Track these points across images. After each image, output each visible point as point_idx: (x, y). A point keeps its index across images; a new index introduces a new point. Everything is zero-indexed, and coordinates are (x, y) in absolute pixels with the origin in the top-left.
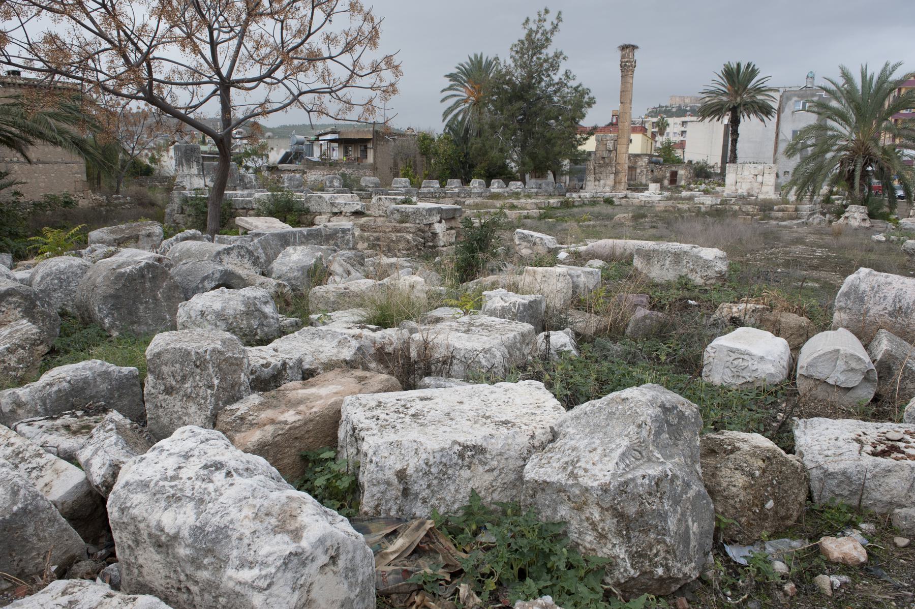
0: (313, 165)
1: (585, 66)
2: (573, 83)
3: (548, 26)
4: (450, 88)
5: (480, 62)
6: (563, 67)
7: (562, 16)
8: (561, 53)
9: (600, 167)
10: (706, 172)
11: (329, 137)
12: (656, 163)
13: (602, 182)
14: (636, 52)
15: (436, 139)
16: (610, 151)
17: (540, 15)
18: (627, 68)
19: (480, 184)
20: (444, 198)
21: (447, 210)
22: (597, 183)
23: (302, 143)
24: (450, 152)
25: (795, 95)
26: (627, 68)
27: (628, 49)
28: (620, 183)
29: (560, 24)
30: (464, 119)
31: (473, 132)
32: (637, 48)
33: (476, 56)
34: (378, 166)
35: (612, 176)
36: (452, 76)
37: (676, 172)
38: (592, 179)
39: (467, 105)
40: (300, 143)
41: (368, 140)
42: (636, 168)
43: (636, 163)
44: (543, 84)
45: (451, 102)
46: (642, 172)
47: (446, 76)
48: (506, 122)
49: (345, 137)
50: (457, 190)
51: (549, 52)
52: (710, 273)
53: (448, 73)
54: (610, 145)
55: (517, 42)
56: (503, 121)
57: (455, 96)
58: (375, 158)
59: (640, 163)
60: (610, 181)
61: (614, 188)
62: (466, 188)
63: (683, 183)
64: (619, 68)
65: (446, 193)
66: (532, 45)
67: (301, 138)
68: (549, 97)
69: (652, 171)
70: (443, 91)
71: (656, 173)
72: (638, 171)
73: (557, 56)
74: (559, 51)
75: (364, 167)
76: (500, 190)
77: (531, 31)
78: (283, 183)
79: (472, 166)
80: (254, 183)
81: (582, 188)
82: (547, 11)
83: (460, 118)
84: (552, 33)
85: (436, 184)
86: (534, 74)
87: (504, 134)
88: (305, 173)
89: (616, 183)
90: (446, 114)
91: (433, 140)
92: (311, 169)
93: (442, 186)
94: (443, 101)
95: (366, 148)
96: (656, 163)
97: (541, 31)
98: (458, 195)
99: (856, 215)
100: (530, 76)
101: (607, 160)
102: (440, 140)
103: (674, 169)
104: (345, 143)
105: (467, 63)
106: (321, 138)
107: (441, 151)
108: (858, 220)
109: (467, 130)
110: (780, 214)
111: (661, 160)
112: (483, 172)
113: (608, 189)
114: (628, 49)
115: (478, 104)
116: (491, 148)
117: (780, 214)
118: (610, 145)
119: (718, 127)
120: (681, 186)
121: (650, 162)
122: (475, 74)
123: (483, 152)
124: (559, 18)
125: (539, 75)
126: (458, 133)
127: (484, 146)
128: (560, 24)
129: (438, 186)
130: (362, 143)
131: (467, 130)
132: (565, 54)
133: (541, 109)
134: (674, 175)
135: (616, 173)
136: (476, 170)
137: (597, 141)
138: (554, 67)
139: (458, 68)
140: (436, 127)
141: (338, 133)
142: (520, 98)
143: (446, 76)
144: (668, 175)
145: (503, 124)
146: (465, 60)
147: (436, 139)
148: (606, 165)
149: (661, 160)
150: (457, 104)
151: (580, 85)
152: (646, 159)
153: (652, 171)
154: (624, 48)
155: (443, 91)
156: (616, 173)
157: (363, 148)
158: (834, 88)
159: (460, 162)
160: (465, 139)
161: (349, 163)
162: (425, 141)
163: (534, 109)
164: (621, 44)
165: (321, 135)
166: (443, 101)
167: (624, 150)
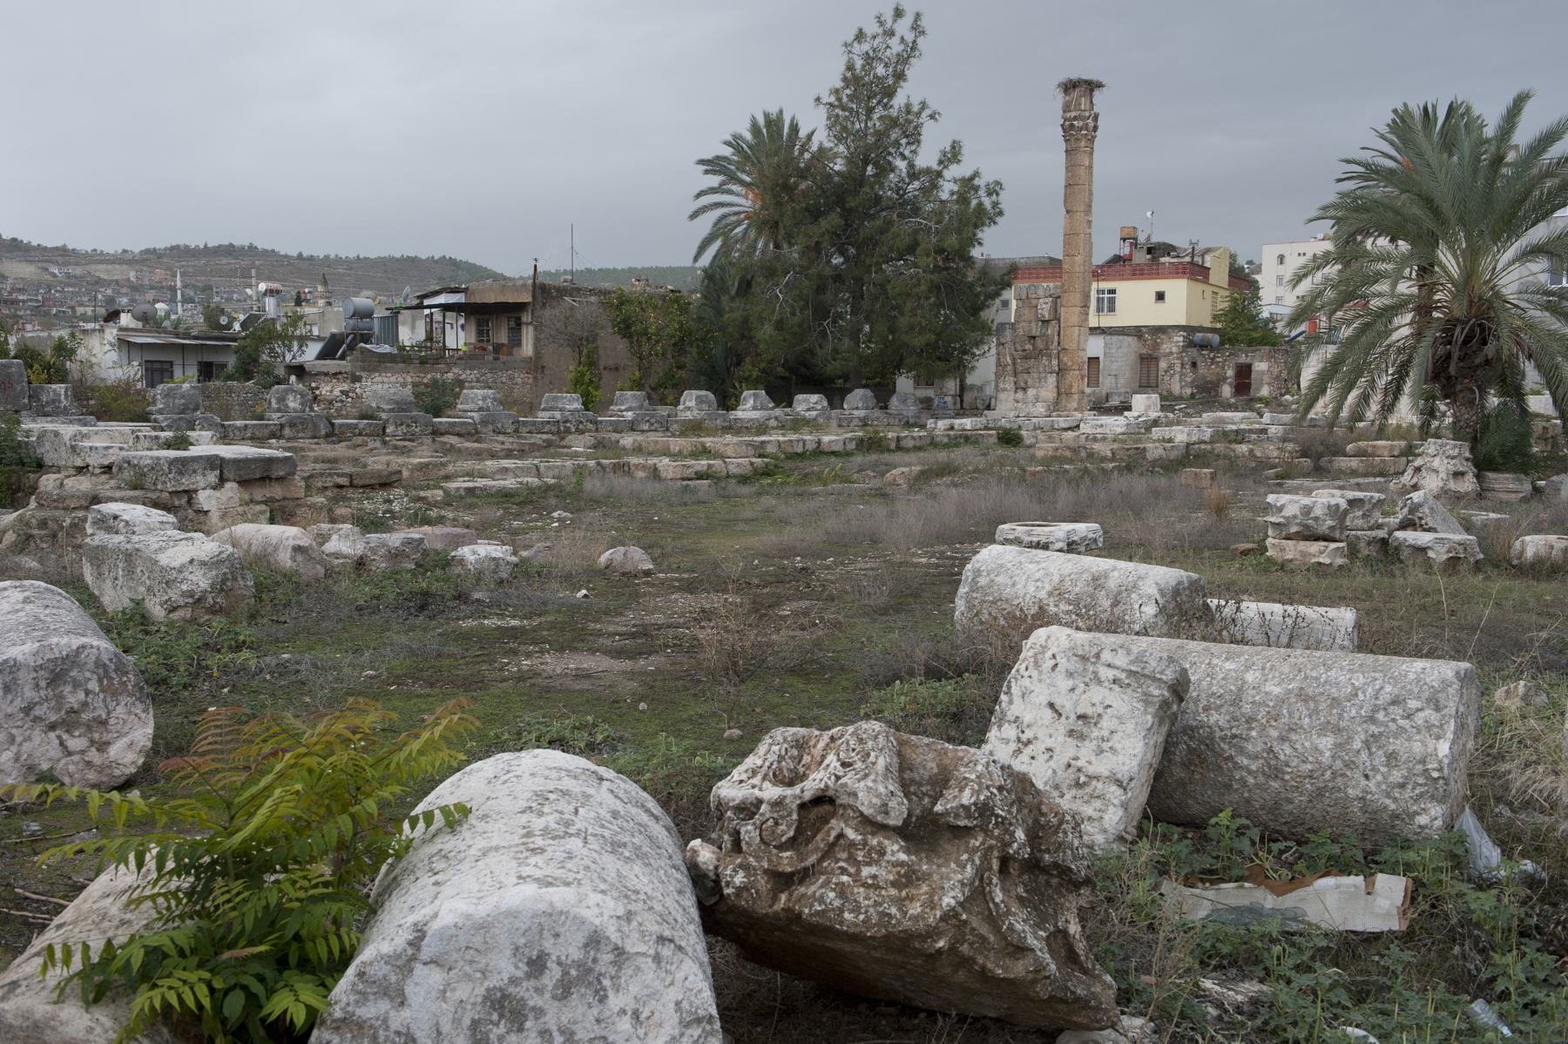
0: (379, 363)
1: (981, 131)
7: (923, 23)
8: (924, 106)
9: (1026, 358)
11: (442, 299)
12: (1203, 346)
13: (1031, 392)
14: (1098, 96)
17: (881, 23)
18: (1079, 133)
19: (700, 400)
21: (236, 462)
22: (1020, 395)
23: (368, 314)
26: (1079, 133)
29: (920, 40)
32: (1100, 85)
35: (1052, 379)
36: (713, 165)
41: (520, 307)
42: (1156, 359)
43: (1156, 346)
46: (1171, 367)
49: (478, 299)
50: (629, 415)
52: (174, 595)
53: (709, 156)
57: (722, 205)
59: (1166, 347)
60: (1048, 390)
61: (1056, 406)
63: (1265, 391)
66: (868, 89)
69: (1194, 365)
70: (699, 195)
71: (1202, 370)
72: (1163, 365)
78: (154, 402)
80: (64, 403)
82: (898, 13)
86: (873, 153)
88: (359, 379)
89: (1062, 393)
92: (371, 370)
95: (519, 324)
96: (1203, 346)
99: (1436, 463)
101: (1040, 344)
103: (1243, 359)
104: (480, 314)
106: (426, 302)
108: (1443, 475)
110: (1354, 463)
111: (1216, 338)
113: (1040, 409)
114: (1080, 88)
117: (1354, 463)
118: (1045, 308)
120: (1260, 400)
121: (1190, 344)
122: (767, 157)
124: (916, 28)
129: (577, 405)
130: (511, 312)
132: (933, 105)
134: (1244, 372)
135: (1061, 372)
141: (465, 291)
143: (702, 162)
144: (1230, 373)
148: (1037, 354)
149: (1216, 338)
152: (1179, 339)
153: (1194, 365)
154: (1069, 86)
155: (699, 195)
156: (1061, 372)
157: (513, 324)
158: (1362, 170)
165: (426, 296)
167: (1075, 319)
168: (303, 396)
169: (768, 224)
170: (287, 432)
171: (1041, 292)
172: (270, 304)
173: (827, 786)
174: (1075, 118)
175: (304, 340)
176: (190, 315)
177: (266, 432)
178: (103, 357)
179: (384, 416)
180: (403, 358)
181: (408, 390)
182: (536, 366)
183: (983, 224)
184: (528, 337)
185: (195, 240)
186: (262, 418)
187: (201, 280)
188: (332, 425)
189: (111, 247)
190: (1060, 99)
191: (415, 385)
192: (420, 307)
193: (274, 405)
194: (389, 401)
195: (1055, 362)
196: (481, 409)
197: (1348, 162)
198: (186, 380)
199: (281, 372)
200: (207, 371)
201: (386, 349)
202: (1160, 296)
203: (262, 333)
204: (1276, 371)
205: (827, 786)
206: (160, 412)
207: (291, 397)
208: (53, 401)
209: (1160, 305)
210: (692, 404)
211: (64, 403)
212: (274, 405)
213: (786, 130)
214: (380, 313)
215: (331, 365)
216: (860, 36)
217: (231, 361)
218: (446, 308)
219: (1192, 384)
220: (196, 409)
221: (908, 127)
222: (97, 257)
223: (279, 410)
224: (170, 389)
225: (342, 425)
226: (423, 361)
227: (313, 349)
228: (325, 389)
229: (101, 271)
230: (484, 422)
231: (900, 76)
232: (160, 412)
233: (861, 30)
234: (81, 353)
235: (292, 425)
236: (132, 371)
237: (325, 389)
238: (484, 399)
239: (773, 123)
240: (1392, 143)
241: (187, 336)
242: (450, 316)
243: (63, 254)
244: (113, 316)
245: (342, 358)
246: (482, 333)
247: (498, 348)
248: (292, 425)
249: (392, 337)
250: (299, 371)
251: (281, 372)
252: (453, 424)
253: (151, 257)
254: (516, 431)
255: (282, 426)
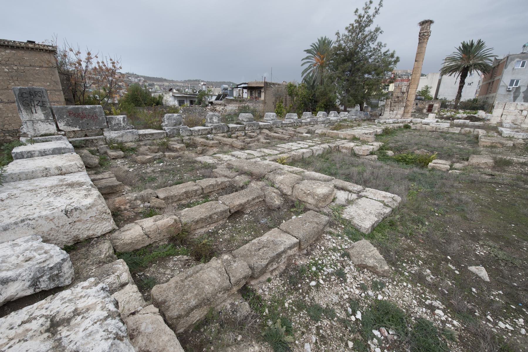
1: (396, 39)
2: (383, 50)
3: (371, 12)
4: (307, 58)
5: (324, 42)
6: (380, 38)
10: (445, 105)
11: (242, 86)
12: (420, 99)
13: (395, 112)
15: (298, 86)
16: (403, 93)
17: (366, 5)
18: (423, 37)
19: (324, 115)
20: (300, 127)
22: (391, 112)
23: (226, 89)
24: (304, 94)
25: (518, 57)
26: (423, 37)
27: (426, 24)
28: (408, 113)
30: (313, 75)
31: (317, 83)
32: (431, 22)
33: (322, 38)
34: (267, 101)
35: (403, 109)
36: (308, 51)
37: (432, 105)
38: (388, 110)
39: (315, 67)
40: (226, 89)
41: (261, 88)
44: (364, 50)
45: (307, 65)
47: (305, 51)
48: (340, 75)
49: (250, 86)
50: (309, 120)
51: (372, 28)
54: (404, 89)
55: (348, 26)
56: (338, 75)
58: (265, 97)
61: (403, 116)
62: (315, 118)
64: (418, 37)
65: (301, 123)
66: (360, 25)
67: (226, 86)
68: (367, 59)
69: (417, 104)
71: (419, 105)
73: (377, 30)
74: (378, 27)
75: (259, 102)
76: (335, 118)
77: (360, 17)
79: (316, 102)
80: (123, 124)
81: (381, 115)
82: (371, 2)
83: (311, 75)
84: (374, 16)
85: (295, 116)
87: (338, 83)
88: (225, 106)
90: (303, 73)
91: (296, 87)
92: (229, 103)
93: (299, 117)
94: (302, 65)
95: (261, 92)
96: (420, 99)
97: (366, 16)
98: (309, 123)
100: (356, 45)
101: (400, 99)
102: (300, 87)
103: (431, 103)
105: (317, 43)
107: (300, 93)
109: (314, 82)
112: (323, 105)
113: (399, 116)
114: (426, 24)
115: (322, 66)
116: (330, 91)
118: (404, 89)
119: (456, 77)
122: (321, 49)
123: (324, 94)
125: (362, 45)
126: (310, 84)
127: (325, 89)
128: (381, 8)
129: (297, 117)
131: (314, 82)
132: (382, 29)
133: (362, 67)
135: (406, 107)
136: (319, 104)
137: (395, 86)
138: (373, 39)
139: (312, 46)
140: (298, 80)
142: (349, 60)
143: (305, 51)
144: (427, 106)
145: (338, 77)
146: (316, 41)
147: (298, 86)
148: (399, 102)
150: (310, 67)
151: (388, 51)
153: (417, 104)
156: (406, 107)
159: (310, 99)
160: (313, 87)
161: (251, 100)
162: (291, 89)
163: (358, 67)
164: (422, 20)
166: (302, 65)
168: (218, 117)
170: (214, 131)
171: (403, 84)
172: (204, 87)
174: (425, 32)
175: (212, 96)
176: (189, 91)
177: (206, 132)
178: (170, 100)
179: (245, 123)
180: (235, 100)
181: (237, 108)
182: (264, 102)
184: (263, 95)
185: (192, 79)
186: (204, 126)
187: (193, 85)
188: (229, 127)
189: (179, 80)
191: (239, 107)
192: (238, 87)
193: (209, 121)
194: (246, 118)
195: (404, 104)
196: (272, 120)
198: (187, 103)
199: (207, 103)
200: (192, 102)
201: (232, 98)
203: (203, 94)
206: (166, 126)
207: (214, 118)
208: (118, 124)
210: (321, 115)
211: (123, 124)
212: (209, 121)
214: (229, 89)
215: (219, 102)
217: (197, 100)
218: (244, 88)
219: (415, 109)
220: (180, 124)
222: (177, 82)
223: (210, 123)
224: (170, 116)
225: (232, 128)
226: (240, 101)
227: (214, 98)
228: (218, 108)
229: (178, 84)
230: (273, 124)
232: (166, 126)
233: (357, 9)
234: (165, 98)
235: (215, 128)
236: (176, 103)
237: (218, 108)
238: (273, 116)
241: (187, 94)
242: (245, 91)
243: (172, 81)
244: (171, 90)
245: (221, 100)
246: (251, 94)
247: (256, 98)
248: (215, 129)
249: (232, 95)
250: (211, 103)
251: (207, 103)
252: (265, 125)
253: (185, 82)
254: (282, 126)
255: (212, 129)
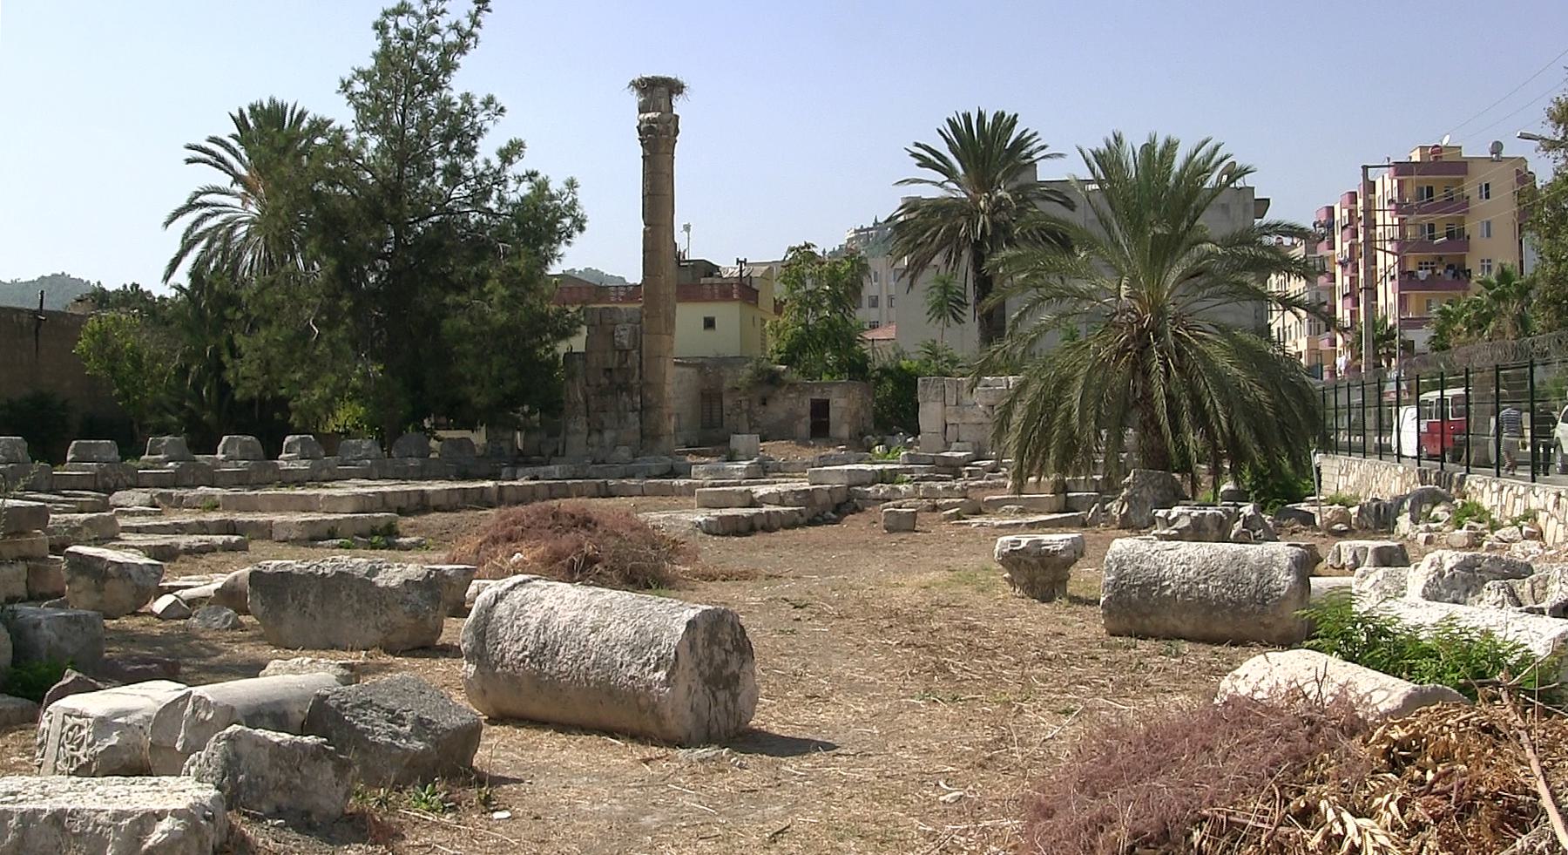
13: (608, 435)
18: (658, 140)
22: (595, 438)
26: (658, 140)
66: (407, 73)
169: (278, 236)
173: (37, 626)
183: (786, 265)
190: (634, 99)
197: (190, 147)
202: (709, 323)
204: (854, 408)
205: (37, 626)
209: (709, 332)
213: (1012, 139)
216: (402, 10)
221: (459, 131)
231: (447, 67)
239: (1004, 123)
240: (1183, 170)
